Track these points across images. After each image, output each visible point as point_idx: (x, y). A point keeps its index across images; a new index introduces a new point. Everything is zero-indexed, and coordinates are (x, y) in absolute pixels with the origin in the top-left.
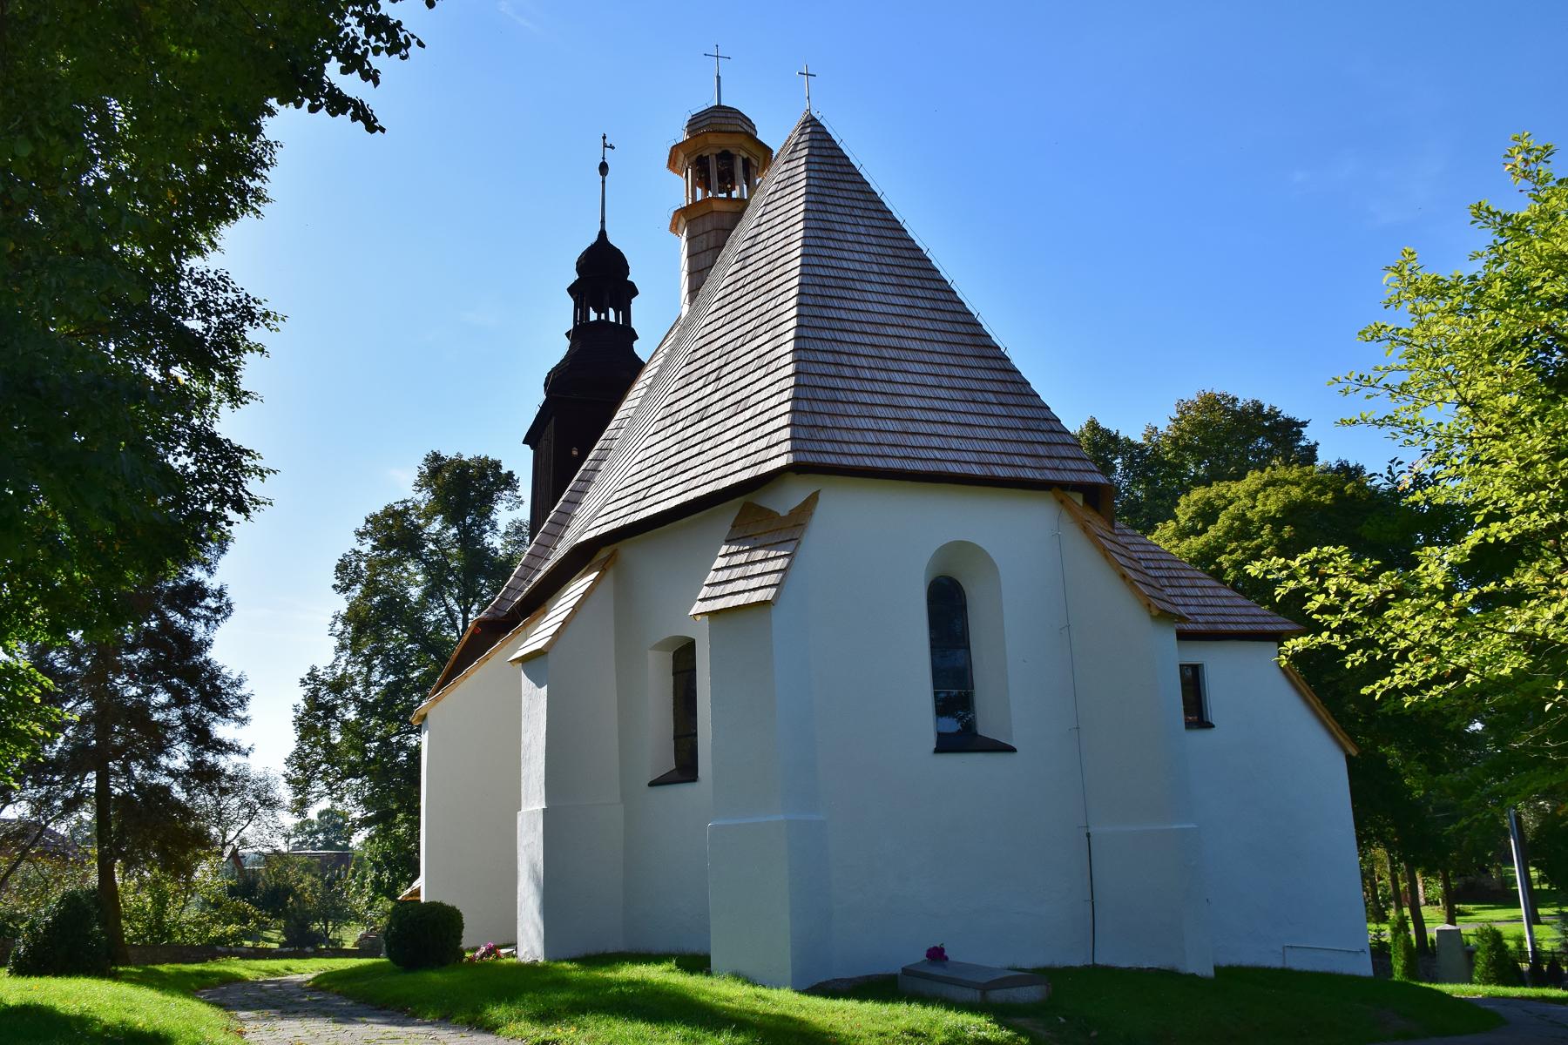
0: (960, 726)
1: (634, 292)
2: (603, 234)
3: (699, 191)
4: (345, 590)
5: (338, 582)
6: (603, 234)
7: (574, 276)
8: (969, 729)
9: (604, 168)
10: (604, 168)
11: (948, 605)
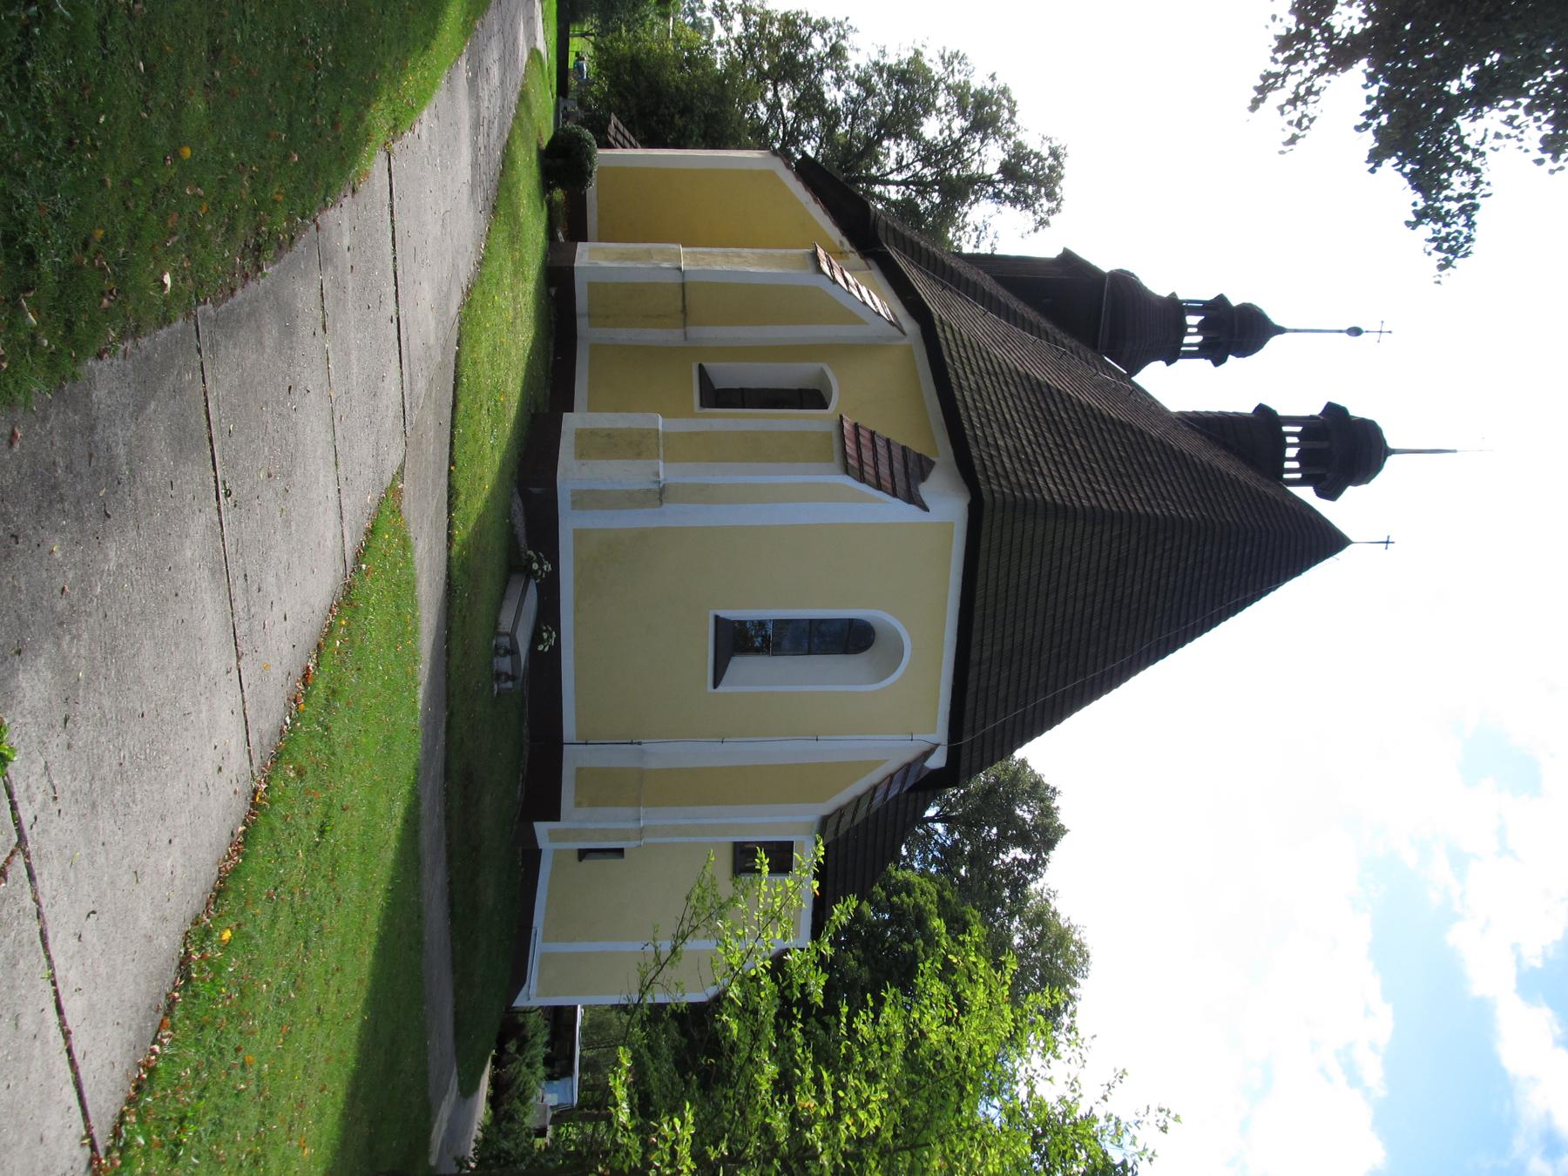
0: (735, 640)
2: (1281, 330)
3: (1298, 429)
6: (1281, 330)
7: (1235, 302)
9: (1355, 331)
10: (1355, 331)
11: (851, 638)
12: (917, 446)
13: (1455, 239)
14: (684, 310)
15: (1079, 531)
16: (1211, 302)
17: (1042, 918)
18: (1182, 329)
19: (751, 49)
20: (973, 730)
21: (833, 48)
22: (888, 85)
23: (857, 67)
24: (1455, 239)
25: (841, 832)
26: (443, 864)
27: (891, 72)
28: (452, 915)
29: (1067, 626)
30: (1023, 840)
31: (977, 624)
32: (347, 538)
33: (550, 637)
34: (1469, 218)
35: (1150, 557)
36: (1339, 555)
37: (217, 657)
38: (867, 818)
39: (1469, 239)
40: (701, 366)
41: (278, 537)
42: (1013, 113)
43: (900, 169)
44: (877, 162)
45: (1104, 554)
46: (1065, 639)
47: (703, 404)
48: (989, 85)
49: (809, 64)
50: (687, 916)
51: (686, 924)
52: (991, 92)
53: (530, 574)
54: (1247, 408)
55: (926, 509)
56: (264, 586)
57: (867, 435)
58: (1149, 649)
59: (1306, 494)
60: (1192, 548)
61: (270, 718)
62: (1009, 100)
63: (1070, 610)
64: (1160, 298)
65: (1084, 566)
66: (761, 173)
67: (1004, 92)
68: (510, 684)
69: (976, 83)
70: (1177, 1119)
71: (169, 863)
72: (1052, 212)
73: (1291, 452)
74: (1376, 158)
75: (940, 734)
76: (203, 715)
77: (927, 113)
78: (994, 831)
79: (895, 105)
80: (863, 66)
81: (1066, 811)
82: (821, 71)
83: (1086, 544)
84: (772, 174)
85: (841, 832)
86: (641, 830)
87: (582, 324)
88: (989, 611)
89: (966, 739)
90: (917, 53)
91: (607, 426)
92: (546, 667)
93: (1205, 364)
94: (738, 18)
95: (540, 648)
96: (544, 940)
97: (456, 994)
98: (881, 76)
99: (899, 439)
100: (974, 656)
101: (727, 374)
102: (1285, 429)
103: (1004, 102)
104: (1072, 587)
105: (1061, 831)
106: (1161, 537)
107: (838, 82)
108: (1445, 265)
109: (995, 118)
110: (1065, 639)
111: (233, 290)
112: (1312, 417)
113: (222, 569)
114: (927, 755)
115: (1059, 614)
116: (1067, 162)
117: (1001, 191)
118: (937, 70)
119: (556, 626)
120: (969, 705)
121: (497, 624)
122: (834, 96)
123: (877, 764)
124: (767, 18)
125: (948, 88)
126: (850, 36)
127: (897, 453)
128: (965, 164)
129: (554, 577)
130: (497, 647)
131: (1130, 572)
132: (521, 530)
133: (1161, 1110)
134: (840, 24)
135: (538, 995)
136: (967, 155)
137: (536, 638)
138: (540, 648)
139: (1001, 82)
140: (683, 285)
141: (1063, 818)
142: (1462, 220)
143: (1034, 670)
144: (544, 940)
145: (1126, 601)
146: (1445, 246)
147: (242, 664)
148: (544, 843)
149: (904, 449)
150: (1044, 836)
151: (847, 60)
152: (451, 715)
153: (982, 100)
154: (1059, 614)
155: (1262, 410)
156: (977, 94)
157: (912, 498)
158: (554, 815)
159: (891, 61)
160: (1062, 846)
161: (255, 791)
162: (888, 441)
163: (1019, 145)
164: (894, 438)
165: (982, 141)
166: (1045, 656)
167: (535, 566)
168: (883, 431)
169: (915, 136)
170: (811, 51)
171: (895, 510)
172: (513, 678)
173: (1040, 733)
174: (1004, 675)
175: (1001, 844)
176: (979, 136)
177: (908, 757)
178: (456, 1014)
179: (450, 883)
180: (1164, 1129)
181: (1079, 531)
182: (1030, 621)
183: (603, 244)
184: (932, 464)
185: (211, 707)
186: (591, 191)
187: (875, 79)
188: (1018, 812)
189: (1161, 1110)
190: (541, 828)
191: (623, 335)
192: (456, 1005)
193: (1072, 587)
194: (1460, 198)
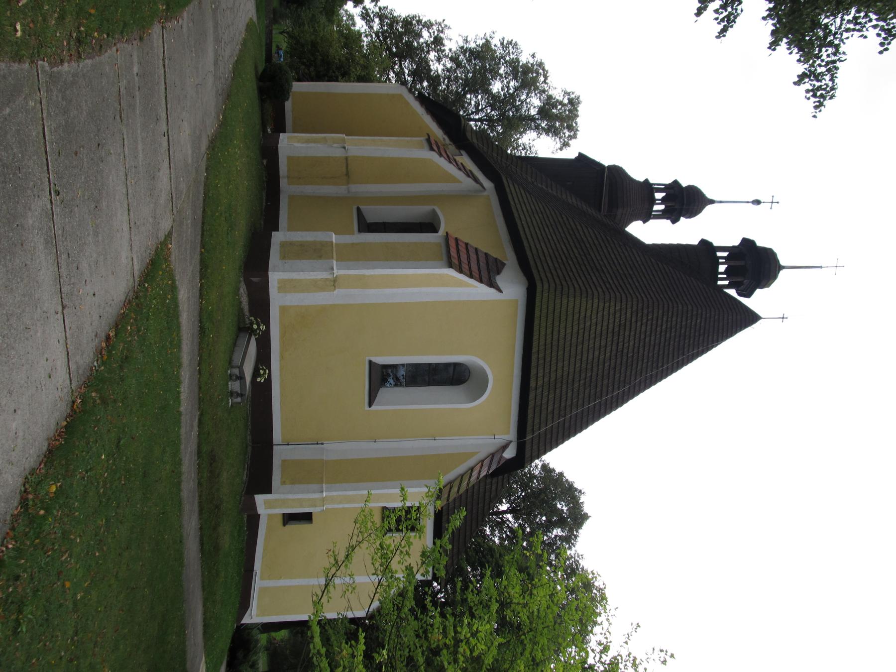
0: (382, 376)
1: (674, 222)
2: (712, 202)
3: (725, 254)
4: (502, 44)
5: (505, 42)
6: (712, 202)
7: (684, 184)
8: (383, 381)
9: (757, 202)
10: (757, 202)
11: (452, 376)
12: (494, 254)
13: (824, 89)
14: (347, 174)
15: (595, 306)
16: (670, 185)
17: (573, 570)
18: (653, 201)
19: (385, 39)
20: (533, 431)
21: (435, 38)
22: (469, 61)
23: (450, 50)
24: (824, 89)
25: (451, 499)
26: (196, 514)
27: (471, 51)
28: (202, 550)
29: (589, 366)
30: (561, 522)
31: (534, 364)
32: (135, 263)
33: (265, 373)
34: (832, 76)
35: (639, 324)
36: (754, 326)
37: (51, 303)
38: (467, 490)
39: (833, 89)
40: (358, 209)
41: (90, 239)
42: (546, 77)
43: (477, 111)
44: (463, 107)
45: (611, 321)
46: (589, 375)
47: (360, 231)
48: (531, 61)
49: (420, 47)
50: (356, 532)
51: (355, 538)
52: (532, 65)
53: (251, 332)
54: (695, 242)
55: (500, 291)
56: (80, 267)
57: (464, 246)
58: (640, 382)
59: (732, 292)
60: (665, 319)
61: (85, 358)
62: (543, 69)
63: (591, 357)
64: (638, 182)
65: (599, 328)
66: (393, 96)
67: (541, 65)
68: (239, 400)
69: (524, 59)
70: (672, 656)
71: (14, 425)
72: (570, 138)
73: (722, 268)
74: (773, 45)
75: (511, 435)
76: (39, 334)
77: (494, 78)
78: (544, 518)
79: (474, 73)
80: (454, 49)
81: (588, 504)
82: (428, 52)
83: (600, 314)
84: (400, 96)
85: (451, 499)
86: (323, 499)
87: (283, 183)
88: (541, 355)
89: (529, 437)
90: (487, 41)
91: (300, 239)
92: (262, 394)
93: (667, 223)
94: (377, 20)
95: (259, 380)
96: (262, 579)
97: (204, 606)
98: (465, 55)
99: (484, 248)
100: (532, 384)
101: (374, 214)
102: (719, 254)
103: (541, 71)
104: (592, 342)
105: (585, 517)
106: (645, 311)
107: (439, 60)
108: (819, 106)
109: (535, 80)
110: (589, 375)
111: (62, 61)
112: (734, 247)
113: (52, 242)
114: (504, 448)
115: (584, 359)
116: (581, 109)
117: (539, 125)
118: (500, 51)
119: (269, 368)
120: (530, 416)
121: (230, 361)
122: (437, 67)
123: (472, 454)
124: (394, 20)
125: (506, 62)
126: (446, 31)
127: (481, 255)
128: (518, 109)
129: (267, 333)
130: (231, 376)
131: (627, 333)
132: (245, 300)
133: (662, 651)
134: (440, 24)
135: (257, 616)
136: (518, 103)
137: (256, 373)
138: (259, 380)
139: (538, 58)
140: (347, 158)
141: (586, 509)
142: (828, 78)
143: (569, 394)
144: (262, 579)
145: (625, 351)
146: (819, 93)
147: (65, 311)
148: (261, 510)
149: (486, 254)
150: (577, 518)
151: (444, 46)
152: (201, 415)
153: (527, 69)
154: (584, 359)
155: (704, 243)
156: (525, 66)
157: (492, 284)
158: (268, 490)
159: (472, 45)
160: (587, 525)
161: (73, 402)
162: (476, 249)
163: (550, 97)
164: (480, 247)
165: (527, 95)
166: (576, 385)
167: (255, 327)
168: (473, 243)
169: (487, 92)
170: (422, 40)
171: (479, 291)
172: (242, 395)
173: (575, 434)
174: (551, 396)
175: (548, 526)
176: (525, 92)
177: (492, 449)
178: (205, 620)
179: (201, 529)
180: (664, 662)
181: (595, 306)
182: (566, 363)
183: (296, 134)
184: (504, 265)
185: (44, 331)
186: (288, 105)
187: (461, 57)
188: (559, 506)
189: (662, 651)
190: (260, 499)
191: (309, 189)
192: (205, 614)
193: (592, 342)
194: (828, 63)
